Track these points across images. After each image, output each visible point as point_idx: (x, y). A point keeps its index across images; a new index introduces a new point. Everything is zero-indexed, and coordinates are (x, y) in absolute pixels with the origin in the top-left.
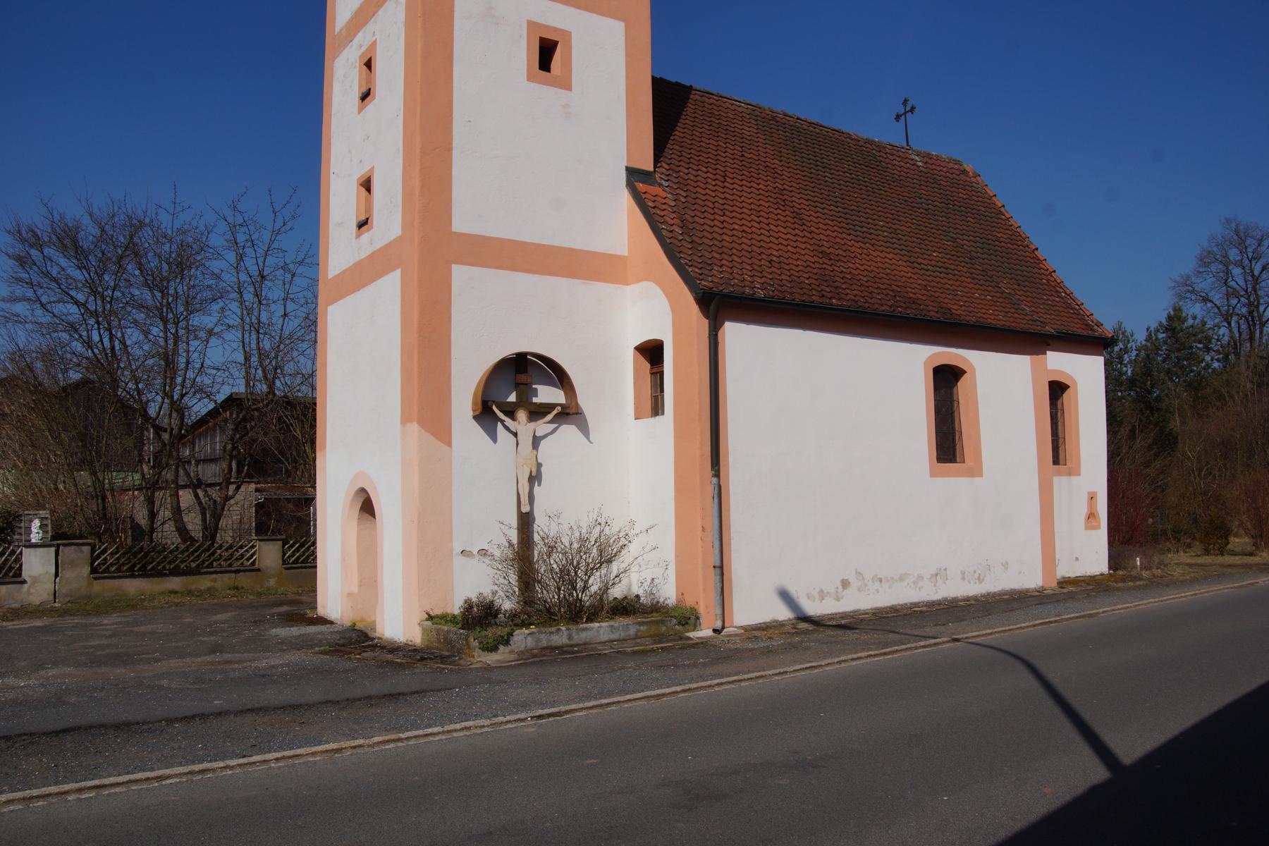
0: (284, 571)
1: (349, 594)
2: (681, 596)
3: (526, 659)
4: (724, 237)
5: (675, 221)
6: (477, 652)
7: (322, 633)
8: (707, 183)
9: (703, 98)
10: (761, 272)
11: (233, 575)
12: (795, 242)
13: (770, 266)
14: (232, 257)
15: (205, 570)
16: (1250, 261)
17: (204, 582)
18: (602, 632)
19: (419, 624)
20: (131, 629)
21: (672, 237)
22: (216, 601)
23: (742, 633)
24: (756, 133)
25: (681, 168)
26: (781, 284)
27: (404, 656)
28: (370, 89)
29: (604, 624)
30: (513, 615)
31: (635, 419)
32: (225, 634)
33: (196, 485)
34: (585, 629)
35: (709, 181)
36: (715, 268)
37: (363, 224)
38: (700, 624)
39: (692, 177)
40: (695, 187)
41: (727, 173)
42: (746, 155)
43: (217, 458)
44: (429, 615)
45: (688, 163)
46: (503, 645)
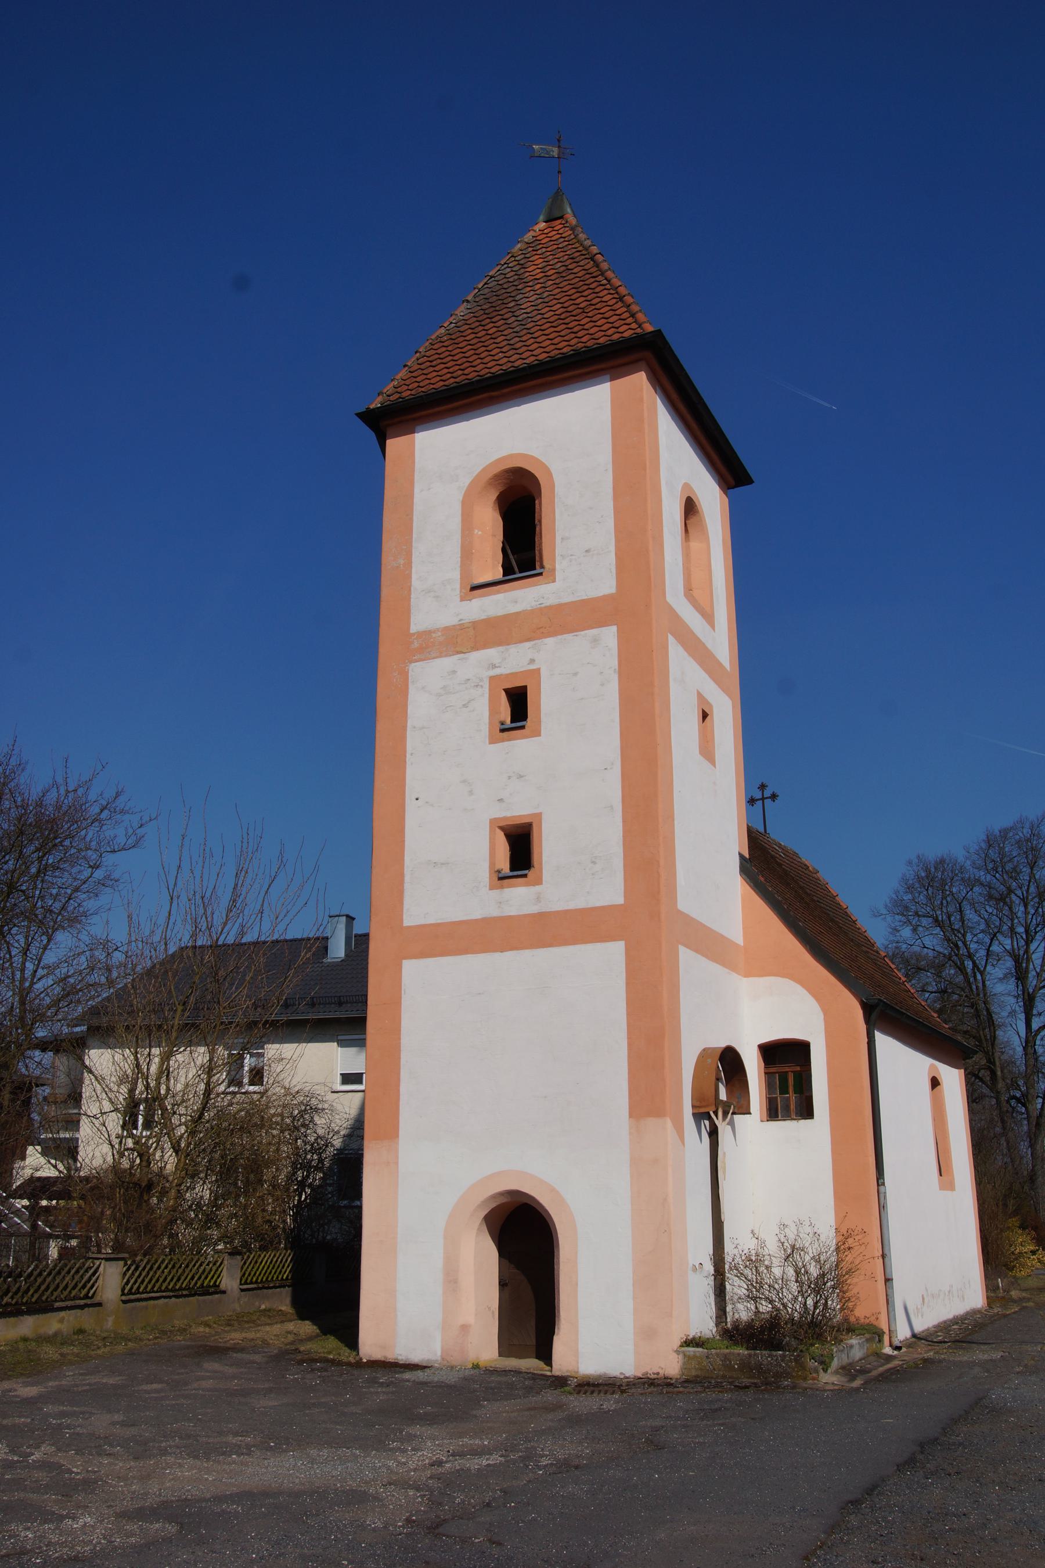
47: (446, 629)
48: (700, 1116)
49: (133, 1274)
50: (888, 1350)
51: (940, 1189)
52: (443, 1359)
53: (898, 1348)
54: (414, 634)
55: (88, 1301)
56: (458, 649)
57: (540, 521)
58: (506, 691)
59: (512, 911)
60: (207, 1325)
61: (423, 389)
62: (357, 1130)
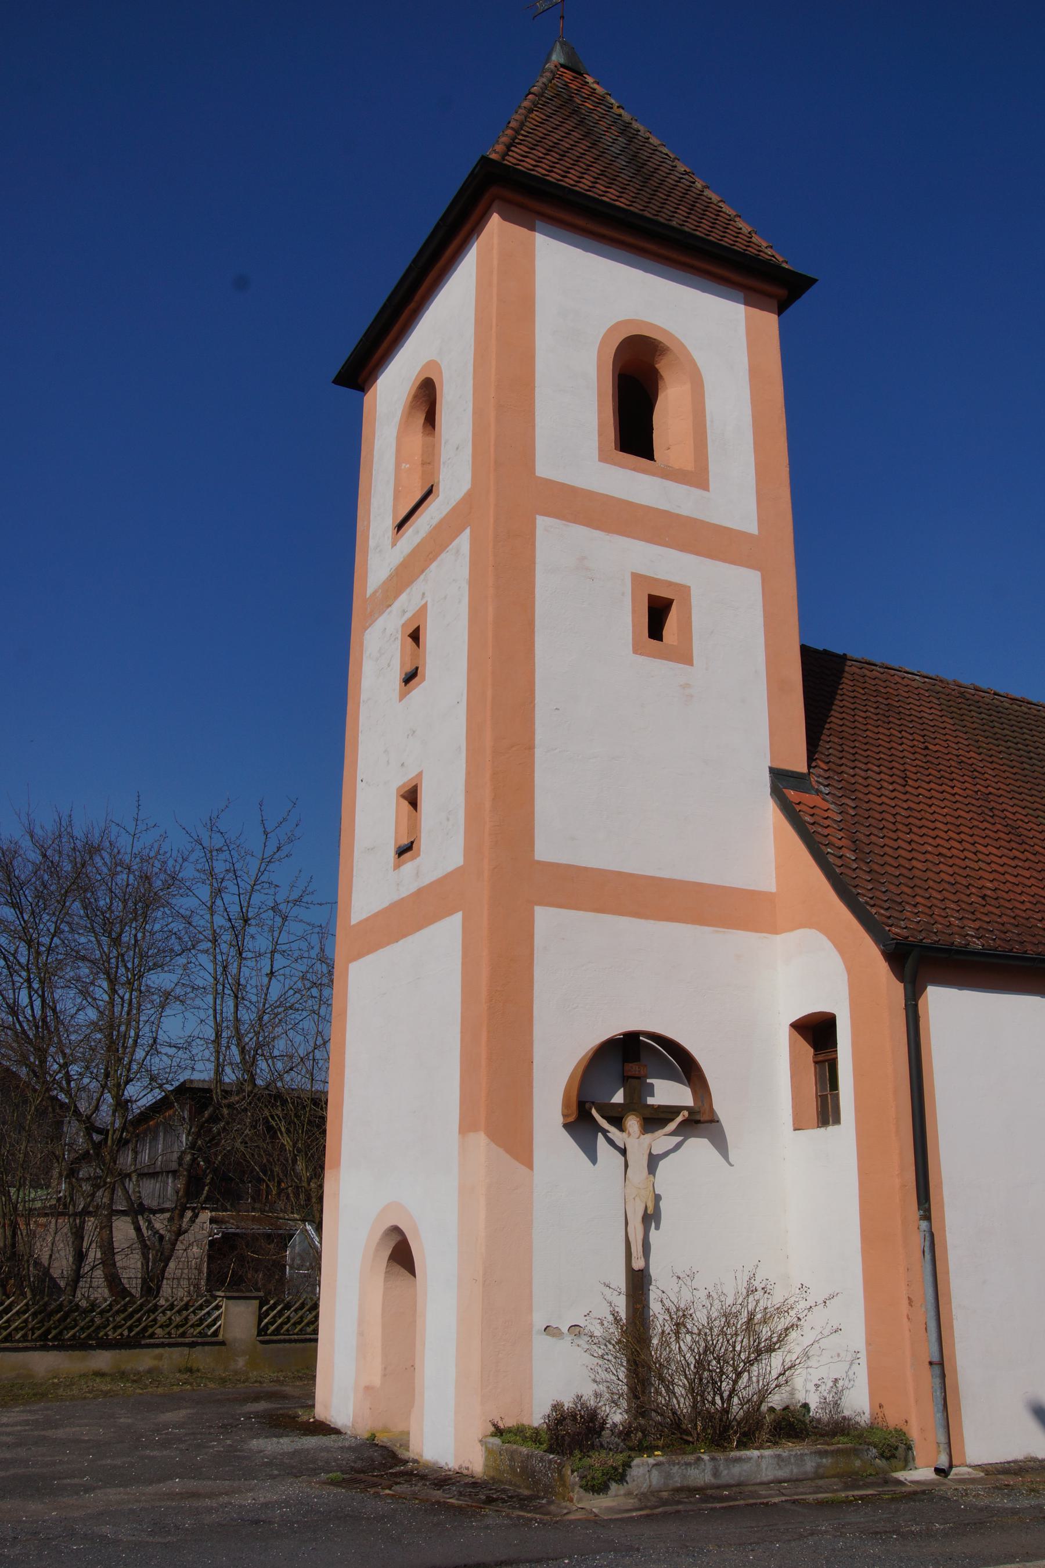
0: (261, 1346)
1: (367, 1388)
2: (878, 1410)
3: (652, 1508)
4: (914, 863)
5: (844, 842)
6: (577, 1493)
7: (327, 1449)
8: (882, 787)
9: (863, 670)
10: (973, 913)
11: (186, 1350)
12: (1015, 867)
13: (984, 903)
14: (204, 892)
15: (148, 1341)
17: (143, 1360)
18: (764, 1465)
19: (481, 1441)
20: (43, 1433)
21: (842, 865)
22: (160, 1390)
23: (981, 1478)
24: (941, 716)
25: (843, 768)
26: (1003, 928)
27: (460, 1494)
28: (417, 668)
29: (767, 1453)
30: (626, 1433)
31: (795, 1130)
32: (183, 1446)
33: (137, 1210)
34: (738, 1460)
35: (885, 785)
36: (908, 908)
37: (404, 850)
38: (914, 1459)
39: (861, 780)
40: (867, 794)
41: (908, 773)
42: (931, 747)
43: (158, 1173)
44: (495, 1425)
45: (853, 761)
46: (616, 1482)
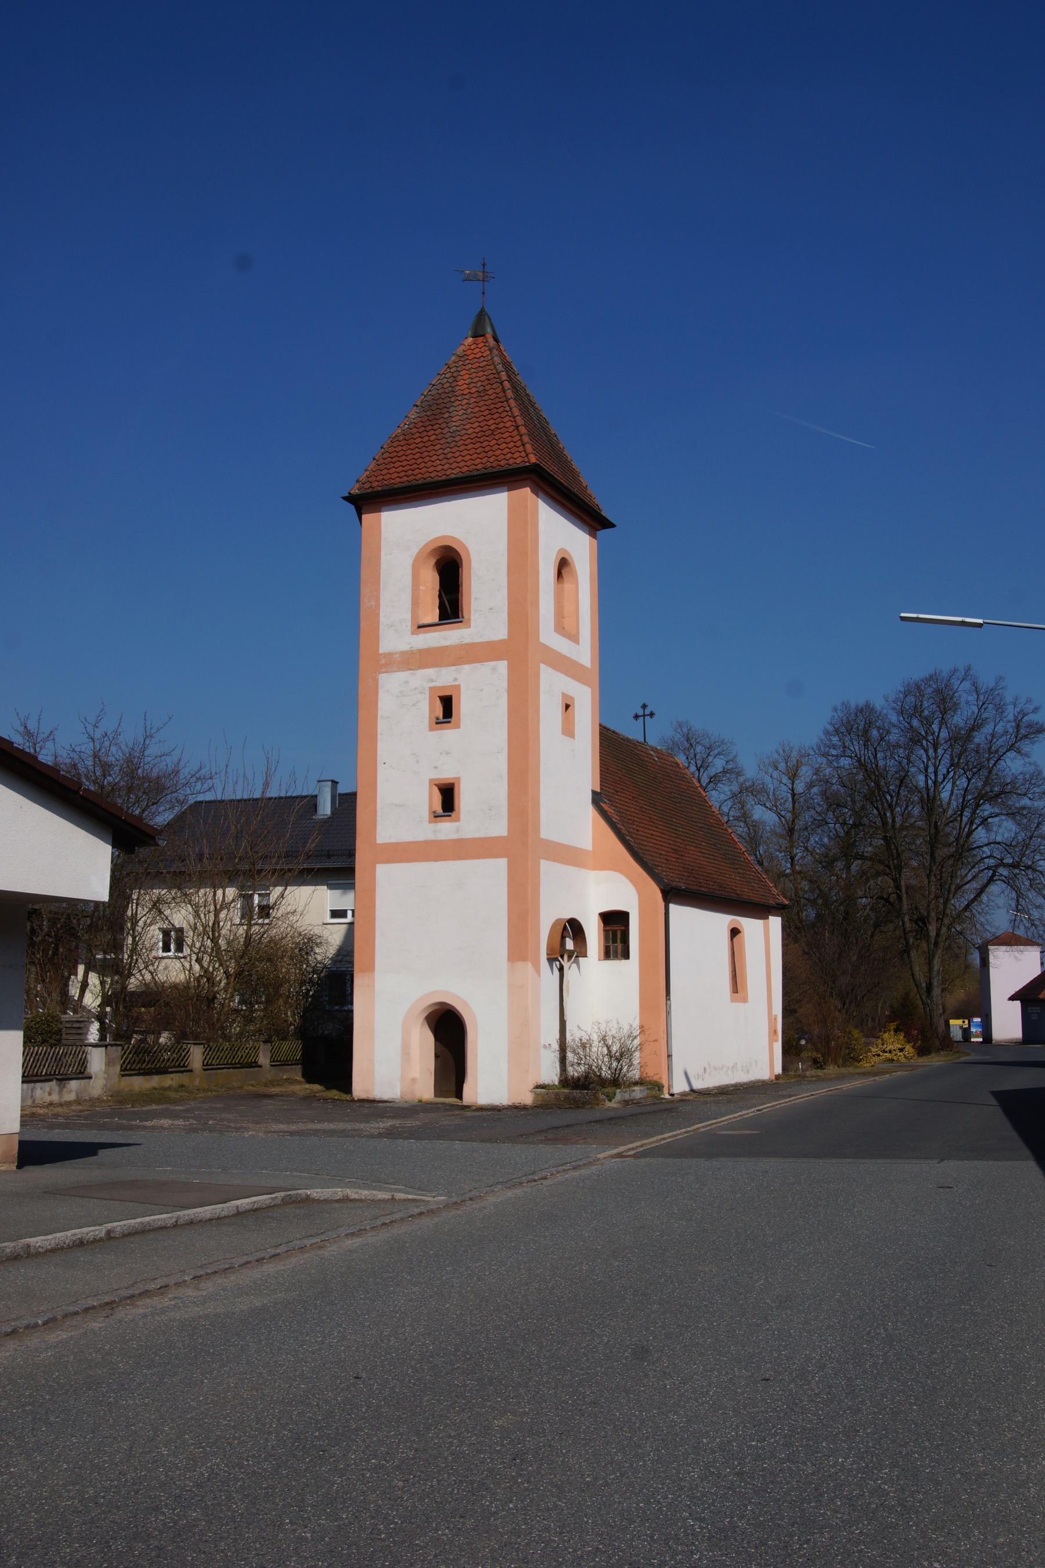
16: (699, 770)
47: (403, 653)
48: (551, 960)
49: (208, 1054)
50: (667, 1096)
51: (732, 1001)
52: (401, 1097)
53: (672, 1095)
54: (382, 654)
55: (185, 1069)
56: (411, 667)
57: (462, 584)
58: (440, 697)
59: (442, 837)
60: (253, 1086)
61: (386, 482)
62: (346, 953)
